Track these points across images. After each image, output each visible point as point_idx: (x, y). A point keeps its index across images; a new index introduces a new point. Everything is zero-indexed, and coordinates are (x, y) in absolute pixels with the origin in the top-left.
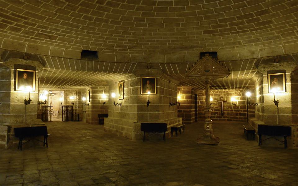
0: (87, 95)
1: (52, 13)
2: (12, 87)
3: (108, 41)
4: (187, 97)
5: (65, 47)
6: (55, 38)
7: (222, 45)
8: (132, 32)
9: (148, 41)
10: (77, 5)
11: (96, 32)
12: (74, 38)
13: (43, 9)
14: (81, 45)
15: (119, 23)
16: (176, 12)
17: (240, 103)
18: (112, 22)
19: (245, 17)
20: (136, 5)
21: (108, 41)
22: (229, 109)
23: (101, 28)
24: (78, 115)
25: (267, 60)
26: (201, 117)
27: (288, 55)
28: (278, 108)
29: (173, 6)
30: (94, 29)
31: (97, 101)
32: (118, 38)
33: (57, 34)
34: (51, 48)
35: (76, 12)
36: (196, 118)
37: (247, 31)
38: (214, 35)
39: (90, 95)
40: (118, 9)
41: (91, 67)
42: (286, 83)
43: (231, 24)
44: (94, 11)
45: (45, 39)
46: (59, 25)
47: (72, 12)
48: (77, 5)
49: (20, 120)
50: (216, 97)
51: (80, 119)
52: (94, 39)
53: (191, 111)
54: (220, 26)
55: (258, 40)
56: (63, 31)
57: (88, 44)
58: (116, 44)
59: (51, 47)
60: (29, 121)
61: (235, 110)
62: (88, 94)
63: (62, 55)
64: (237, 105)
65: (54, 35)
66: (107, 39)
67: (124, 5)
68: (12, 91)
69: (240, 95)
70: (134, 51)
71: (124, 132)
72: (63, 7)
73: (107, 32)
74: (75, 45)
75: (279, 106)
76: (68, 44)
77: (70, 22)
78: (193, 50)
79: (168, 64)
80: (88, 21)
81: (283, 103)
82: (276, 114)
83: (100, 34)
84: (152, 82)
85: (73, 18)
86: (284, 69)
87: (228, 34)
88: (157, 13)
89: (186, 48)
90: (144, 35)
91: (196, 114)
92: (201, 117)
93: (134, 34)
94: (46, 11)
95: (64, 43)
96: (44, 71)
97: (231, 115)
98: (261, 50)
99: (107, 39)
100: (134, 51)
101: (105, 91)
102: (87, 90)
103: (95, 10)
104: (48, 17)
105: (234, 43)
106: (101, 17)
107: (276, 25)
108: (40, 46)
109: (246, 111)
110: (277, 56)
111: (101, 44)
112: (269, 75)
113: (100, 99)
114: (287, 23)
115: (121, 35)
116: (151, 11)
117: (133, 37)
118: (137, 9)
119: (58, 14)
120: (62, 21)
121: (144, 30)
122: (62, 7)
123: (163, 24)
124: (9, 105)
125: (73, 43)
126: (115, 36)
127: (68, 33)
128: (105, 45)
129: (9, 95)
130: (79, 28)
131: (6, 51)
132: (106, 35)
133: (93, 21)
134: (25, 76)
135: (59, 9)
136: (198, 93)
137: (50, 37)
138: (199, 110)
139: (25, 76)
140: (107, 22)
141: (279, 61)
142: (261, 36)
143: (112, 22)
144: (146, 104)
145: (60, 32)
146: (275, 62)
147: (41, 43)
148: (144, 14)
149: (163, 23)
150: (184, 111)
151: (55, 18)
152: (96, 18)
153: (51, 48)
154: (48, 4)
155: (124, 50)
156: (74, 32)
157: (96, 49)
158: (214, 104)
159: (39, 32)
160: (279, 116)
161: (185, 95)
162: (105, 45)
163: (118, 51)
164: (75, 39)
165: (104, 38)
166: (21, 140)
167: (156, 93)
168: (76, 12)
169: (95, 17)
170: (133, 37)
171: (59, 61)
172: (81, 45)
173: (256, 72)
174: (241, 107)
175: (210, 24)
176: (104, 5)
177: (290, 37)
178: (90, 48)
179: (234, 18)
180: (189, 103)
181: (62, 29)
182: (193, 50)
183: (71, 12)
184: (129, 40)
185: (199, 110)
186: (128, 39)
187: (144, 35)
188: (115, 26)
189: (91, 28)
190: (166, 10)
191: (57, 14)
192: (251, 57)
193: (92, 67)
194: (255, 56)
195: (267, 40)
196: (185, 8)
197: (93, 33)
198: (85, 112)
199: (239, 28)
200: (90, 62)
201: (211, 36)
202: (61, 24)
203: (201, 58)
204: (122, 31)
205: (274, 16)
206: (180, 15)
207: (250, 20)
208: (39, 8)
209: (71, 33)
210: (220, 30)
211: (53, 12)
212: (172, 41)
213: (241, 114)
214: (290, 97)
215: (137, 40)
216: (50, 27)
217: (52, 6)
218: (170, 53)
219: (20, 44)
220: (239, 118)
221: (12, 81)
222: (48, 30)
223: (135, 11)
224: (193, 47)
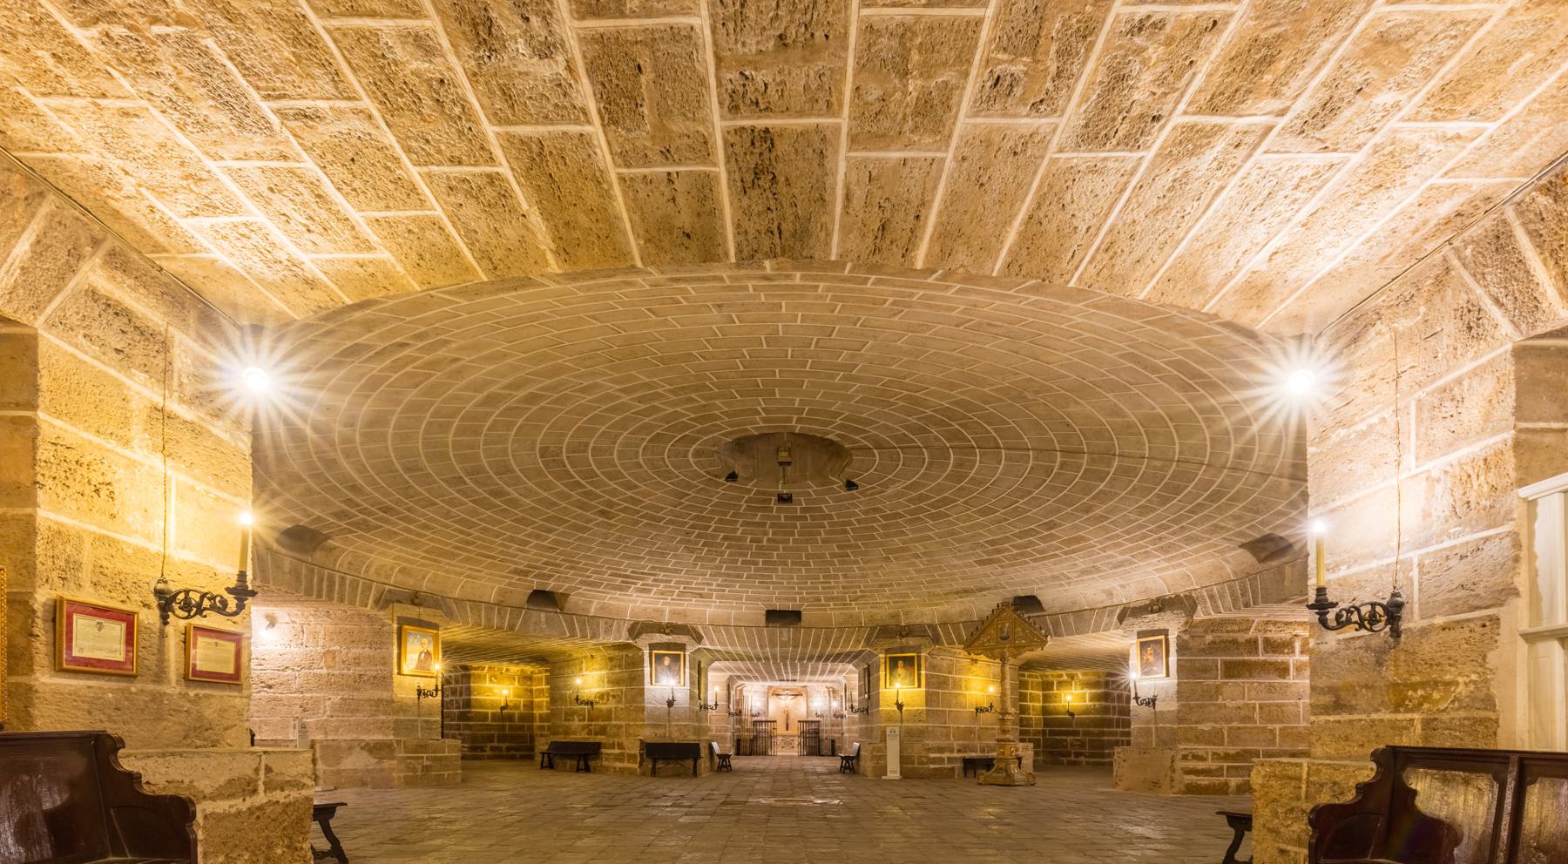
2: (647, 679)
4: (1094, 698)
6: (710, 596)
34: (709, 611)
49: (660, 731)
57: (770, 599)
60: (675, 735)
68: (647, 686)
71: (576, 723)
79: (944, 624)
84: (909, 662)
89: (967, 592)
93: (845, 576)
124: (643, 709)
128: (802, 599)
129: (642, 692)
131: (636, 623)
134: (667, 661)
137: (701, 596)
139: (667, 661)
141: (1160, 610)
146: (1152, 612)
150: (1086, 733)
153: (709, 611)
161: (1088, 692)
166: (655, 761)
180: (1097, 711)
200: (785, 630)
219: (656, 610)
221: (647, 670)
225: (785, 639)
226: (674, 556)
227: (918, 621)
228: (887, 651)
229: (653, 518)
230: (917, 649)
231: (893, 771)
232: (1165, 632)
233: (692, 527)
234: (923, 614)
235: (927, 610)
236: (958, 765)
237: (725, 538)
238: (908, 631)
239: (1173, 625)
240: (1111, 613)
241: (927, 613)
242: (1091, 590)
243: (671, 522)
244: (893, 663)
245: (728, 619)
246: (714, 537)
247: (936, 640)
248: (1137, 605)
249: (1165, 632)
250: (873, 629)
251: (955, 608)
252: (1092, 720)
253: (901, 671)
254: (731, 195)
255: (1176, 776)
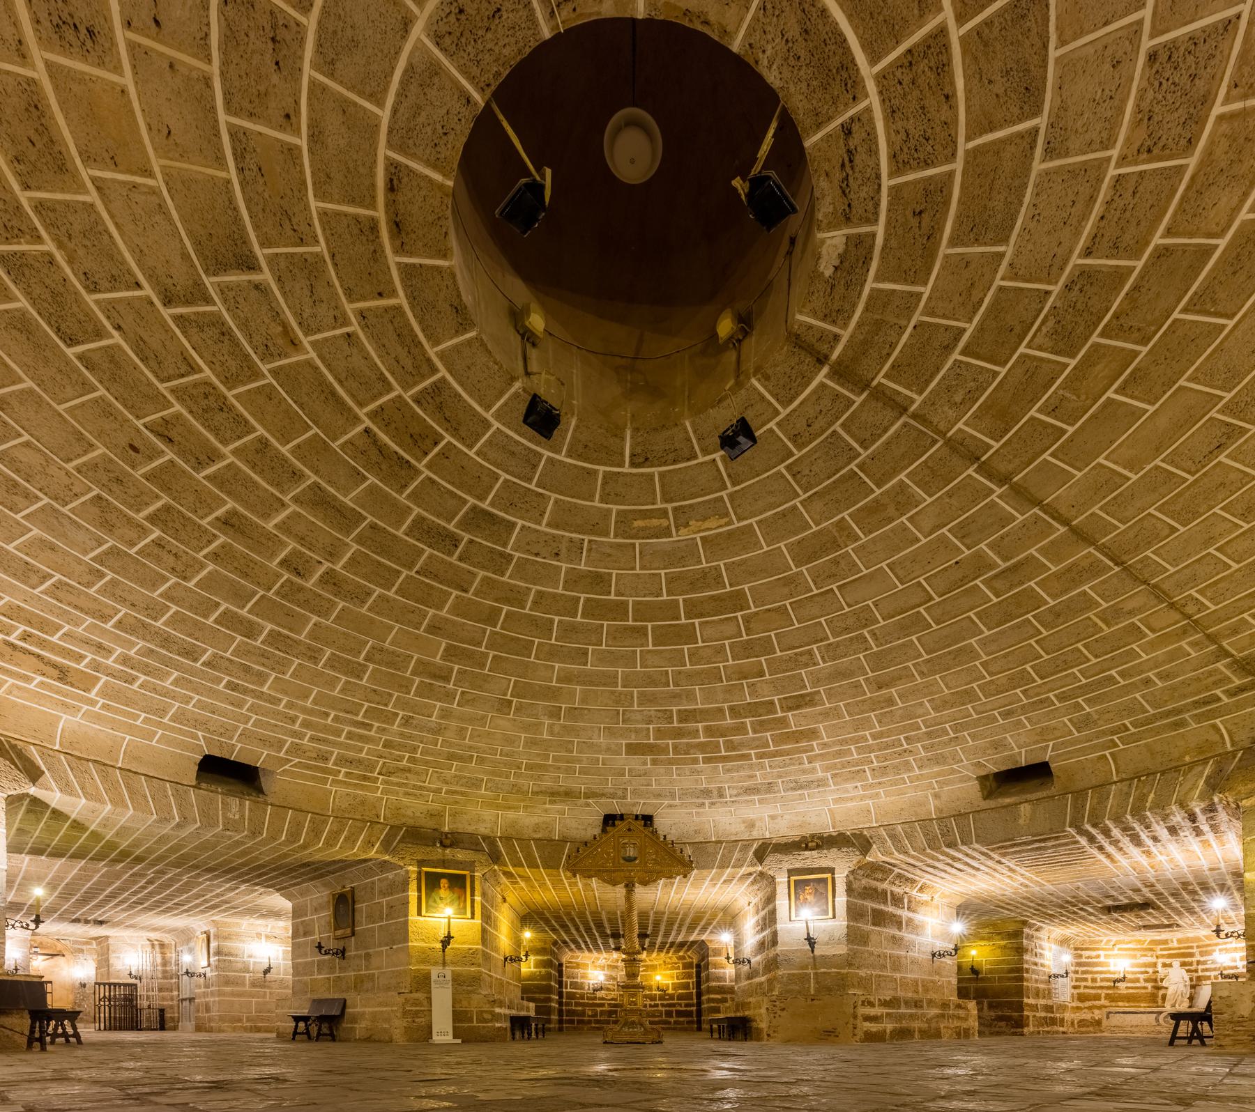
0: (198, 948)
1: (80, 562)
3: (309, 733)
5: (131, 729)
6: (87, 682)
7: (673, 796)
8: (401, 713)
9: (452, 757)
10: (200, 556)
11: (265, 689)
12: (173, 698)
13: (36, 531)
14: (200, 734)
15: (357, 671)
16: (557, 665)
17: (675, 987)
18: (333, 663)
19: (753, 709)
20: (431, 612)
21: (309, 733)
22: (648, 1002)
23: (287, 677)
24: (162, 1011)
25: (786, 844)
26: (572, 1022)
27: (841, 835)
28: (814, 957)
29: (553, 642)
30: (261, 678)
31: (239, 965)
32: (347, 729)
33: (96, 666)
35: (191, 584)
36: (561, 1021)
37: (746, 757)
38: (654, 762)
39: (212, 945)
40: (364, 610)
41: (237, 817)
42: (834, 896)
43: (709, 731)
44: (270, 599)
45: (39, 679)
46: (109, 626)
47: (174, 580)
48: (200, 556)
50: (614, 974)
51: (169, 1024)
52: (255, 717)
53: (549, 1000)
54: (679, 734)
55: (770, 787)
56: (125, 660)
57: (227, 731)
58: (336, 751)
59: (65, 716)
61: (663, 1005)
62: (205, 945)
63: (117, 761)
64: (670, 991)
65: (81, 667)
66: (306, 724)
67: (387, 599)
69: (678, 968)
70: (399, 785)
72: (136, 549)
73: (307, 697)
74: (172, 729)
75: (817, 952)
76: (146, 720)
77: (158, 624)
78: (588, 805)
79: (507, 839)
80: (239, 638)
81: (827, 944)
82: (811, 972)
83: (280, 700)
84: (458, 883)
85: (174, 608)
86: (830, 864)
87: (695, 761)
88: (494, 657)
90: (438, 731)
91: (560, 1012)
92: (572, 1022)
93: (407, 721)
94: (53, 548)
95: (127, 714)
96: (28, 811)
97: (654, 1016)
98: (773, 817)
99: (306, 724)
100: (399, 785)
101: (267, 937)
102: (198, 933)
103: (270, 594)
104: (58, 576)
105: (706, 793)
106: (291, 630)
107: (825, 745)
108: (14, 705)
109: (692, 1005)
110: (813, 836)
111: (281, 744)
112: (793, 878)
113: (252, 960)
114: (855, 741)
115: (359, 718)
116: (479, 644)
117: (402, 735)
118: (434, 629)
119: (110, 575)
120: (124, 611)
121: (445, 714)
122: (132, 544)
123: (510, 702)
125: (166, 720)
126: (336, 719)
127: (147, 670)
128: (296, 750)
130: (196, 660)
131: (482, 159)
132: (305, 710)
133: (258, 643)
135: (113, 552)
136: (564, 960)
137: (63, 674)
138: (567, 1004)
140: (315, 660)
141: (818, 847)
142: (780, 777)
143: (333, 663)
144: (439, 946)
145: (110, 662)
146: (807, 848)
147: (15, 692)
148: (451, 653)
149: (508, 697)
151: (92, 591)
152: (272, 631)
154: (65, 510)
155: (365, 778)
156: (176, 674)
157: (259, 756)
158: (608, 989)
159: (12, 639)
160: (816, 974)
161: (918, 917)
162: (296, 750)
163: (341, 777)
164: (178, 704)
165: (293, 720)
167: (469, 915)
168: (191, 584)
169: (269, 626)
170: (402, 735)
171: (105, 778)
172: (200, 734)
173: (752, 878)
174: (680, 997)
175: (650, 722)
176: (313, 581)
177: (850, 786)
178: (237, 750)
179: (721, 710)
180: (542, 978)
181: (120, 650)
182: (588, 805)
183: (168, 580)
184: (387, 744)
185: (567, 1004)
186: (384, 738)
187: (438, 731)
188: (344, 678)
189: (247, 669)
190: (526, 648)
191: (102, 575)
192: (746, 837)
193: (243, 817)
194: (755, 834)
195: (793, 789)
196: (587, 654)
197: (253, 691)
198: (191, 1000)
199: (731, 746)
200: (234, 802)
201: (645, 763)
202: (119, 624)
203: (604, 831)
204: (367, 704)
205: (826, 715)
206: (566, 678)
207: (762, 723)
208: (18, 523)
209: (162, 676)
210: (675, 747)
211: (86, 559)
212: (530, 767)
213: (679, 1013)
214: (845, 931)
215: (415, 749)
216: (67, 628)
217: (79, 526)
218: (516, 808)
220: (675, 1022)
222: (55, 639)
223: (421, 632)
224: (587, 796)
225: (234, 814)
226: (47, 518)
227: (470, 829)
228: (421, 863)
229: (56, 302)
230: (471, 866)
231: (442, 1029)
232: (831, 871)
233: (165, 430)
234: (480, 820)
235: (488, 814)
236: (507, 1025)
237: (227, 523)
238: (452, 840)
239: (842, 864)
240: (745, 849)
241: (484, 818)
242: (728, 819)
243: (110, 367)
244: (432, 882)
245: (113, 751)
246: (204, 503)
247: (495, 857)
248: (784, 840)
249: (831, 871)
250: (395, 829)
251: (531, 818)
252: (537, 986)
253: (444, 892)
254: (49, 106)
255: (859, 1022)
